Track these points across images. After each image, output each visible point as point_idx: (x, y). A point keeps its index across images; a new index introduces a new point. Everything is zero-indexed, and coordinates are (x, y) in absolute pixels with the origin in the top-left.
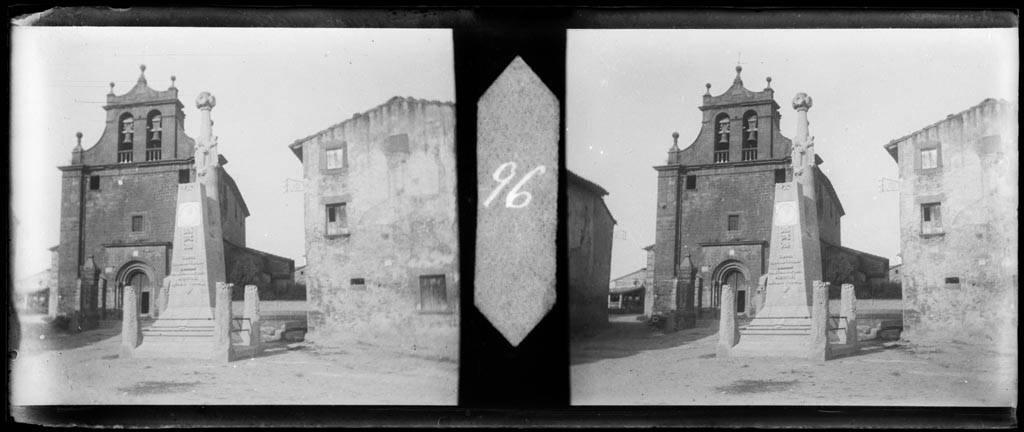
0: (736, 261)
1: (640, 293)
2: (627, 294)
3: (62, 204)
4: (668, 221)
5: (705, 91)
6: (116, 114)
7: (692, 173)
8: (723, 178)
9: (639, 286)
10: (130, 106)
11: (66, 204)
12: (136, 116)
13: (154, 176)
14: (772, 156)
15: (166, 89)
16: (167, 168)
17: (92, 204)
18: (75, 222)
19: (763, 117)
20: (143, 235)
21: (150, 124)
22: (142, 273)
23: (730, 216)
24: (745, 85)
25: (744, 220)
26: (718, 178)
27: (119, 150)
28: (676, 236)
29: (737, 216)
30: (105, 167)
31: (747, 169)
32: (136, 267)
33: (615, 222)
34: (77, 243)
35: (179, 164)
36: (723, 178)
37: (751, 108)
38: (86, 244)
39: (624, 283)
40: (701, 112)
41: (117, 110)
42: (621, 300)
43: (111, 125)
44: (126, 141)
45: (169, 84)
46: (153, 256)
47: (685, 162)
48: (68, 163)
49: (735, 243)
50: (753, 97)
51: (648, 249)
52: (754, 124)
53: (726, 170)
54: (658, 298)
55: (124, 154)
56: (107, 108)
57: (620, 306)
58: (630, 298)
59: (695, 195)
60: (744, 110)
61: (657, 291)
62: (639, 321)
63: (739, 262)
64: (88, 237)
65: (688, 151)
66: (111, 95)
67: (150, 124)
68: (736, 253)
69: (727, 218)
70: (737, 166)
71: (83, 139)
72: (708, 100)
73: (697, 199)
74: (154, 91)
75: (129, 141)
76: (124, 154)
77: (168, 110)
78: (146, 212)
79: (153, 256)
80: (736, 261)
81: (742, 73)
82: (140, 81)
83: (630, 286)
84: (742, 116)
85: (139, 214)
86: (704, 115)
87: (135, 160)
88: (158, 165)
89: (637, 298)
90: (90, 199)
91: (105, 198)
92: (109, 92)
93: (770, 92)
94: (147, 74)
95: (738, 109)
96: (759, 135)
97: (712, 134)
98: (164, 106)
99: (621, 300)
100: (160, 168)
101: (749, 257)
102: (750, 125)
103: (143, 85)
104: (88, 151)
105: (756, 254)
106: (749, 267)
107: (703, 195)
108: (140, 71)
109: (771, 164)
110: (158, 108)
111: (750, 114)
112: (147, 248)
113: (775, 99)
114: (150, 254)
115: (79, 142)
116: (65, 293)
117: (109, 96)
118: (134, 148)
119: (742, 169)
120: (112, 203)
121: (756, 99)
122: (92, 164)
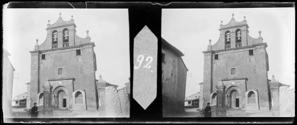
0: (235, 86)
1: (197, 100)
2: (193, 101)
3: (204, 65)
4: (35, 72)
5: (48, 23)
6: (51, 31)
7: (216, 54)
8: (55, 54)
9: (197, 98)
10: (56, 28)
11: (206, 66)
12: (58, 31)
13: (239, 53)
14: (75, 45)
15: (69, 20)
16: (244, 50)
17: (43, 65)
18: (37, 72)
19: (243, 31)
20: (236, 76)
21: (237, 34)
22: (236, 91)
23: (232, 69)
24: (235, 20)
25: (64, 70)
26: (227, 54)
27: (52, 44)
28: (211, 78)
29: (235, 69)
30: (220, 51)
31: (65, 50)
32: (59, 89)
33: (187, 70)
34: (210, 80)
35: (76, 47)
36: (228, 54)
37: (238, 28)
38: (214, 80)
39: (275, 97)
40: (46, 31)
41: (51, 30)
42: (191, 103)
43: (222, 36)
44: (65, 39)
45: (71, 18)
46: (68, 84)
47: (214, 49)
48: (206, 50)
49: (234, 79)
50: (239, 24)
51: (28, 84)
52: (240, 34)
53: (56, 51)
54: (32, 102)
55: (227, 46)
56: (220, 30)
57: (191, 105)
58: (194, 102)
59: (218, 61)
60: (63, 28)
61: (204, 99)
62: (25, 111)
63: (64, 87)
64: (41, 78)
65: (42, 46)
66: (49, 25)
67: (237, 34)
68: (62, 83)
69: (231, 69)
70: (61, 49)
71: (38, 42)
72: (49, 26)
73: (219, 63)
74: (65, 22)
75: (67, 39)
76: (227, 46)
77: (70, 28)
78: (64, 67)
79: (68, 84)
80: (235, 86)
81: (234, 16)
82: (59, 18)
83: (194, 98)
84: (62, 31)
85: (61, 68)
86: (48, 31)
87: (231, 48)
88: (67, 49)
89: (197, 102)
90: (42, 63)
91: (47, 62)
92: (48, 23)
93: (245, 22)
94: (62, 16)
95: (233, 29)
96: (69, 37)
97: (224, 39)
98: (69, 26)
99: (191, 103)
100: (68, 49)
101: (240, 84)
102: (238, 34)
103: (233, 21)
104: (40, 45)
105: (70, 83)
106: (240, 89)
107: (48, 61)
108: (59, 15)
109: (75, 48)
110: (67, 27)
111: (238, 30)
112: (65, 81)
113: (247, 23)
114: (239, 83)
115: (37, 42)
116: (205, 100)
117: (48, 25)
118: (242, 41)
119: (63, 51)
120: (223, 64)
121: (68, 23)
122: (42, 50)
